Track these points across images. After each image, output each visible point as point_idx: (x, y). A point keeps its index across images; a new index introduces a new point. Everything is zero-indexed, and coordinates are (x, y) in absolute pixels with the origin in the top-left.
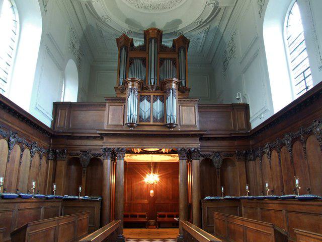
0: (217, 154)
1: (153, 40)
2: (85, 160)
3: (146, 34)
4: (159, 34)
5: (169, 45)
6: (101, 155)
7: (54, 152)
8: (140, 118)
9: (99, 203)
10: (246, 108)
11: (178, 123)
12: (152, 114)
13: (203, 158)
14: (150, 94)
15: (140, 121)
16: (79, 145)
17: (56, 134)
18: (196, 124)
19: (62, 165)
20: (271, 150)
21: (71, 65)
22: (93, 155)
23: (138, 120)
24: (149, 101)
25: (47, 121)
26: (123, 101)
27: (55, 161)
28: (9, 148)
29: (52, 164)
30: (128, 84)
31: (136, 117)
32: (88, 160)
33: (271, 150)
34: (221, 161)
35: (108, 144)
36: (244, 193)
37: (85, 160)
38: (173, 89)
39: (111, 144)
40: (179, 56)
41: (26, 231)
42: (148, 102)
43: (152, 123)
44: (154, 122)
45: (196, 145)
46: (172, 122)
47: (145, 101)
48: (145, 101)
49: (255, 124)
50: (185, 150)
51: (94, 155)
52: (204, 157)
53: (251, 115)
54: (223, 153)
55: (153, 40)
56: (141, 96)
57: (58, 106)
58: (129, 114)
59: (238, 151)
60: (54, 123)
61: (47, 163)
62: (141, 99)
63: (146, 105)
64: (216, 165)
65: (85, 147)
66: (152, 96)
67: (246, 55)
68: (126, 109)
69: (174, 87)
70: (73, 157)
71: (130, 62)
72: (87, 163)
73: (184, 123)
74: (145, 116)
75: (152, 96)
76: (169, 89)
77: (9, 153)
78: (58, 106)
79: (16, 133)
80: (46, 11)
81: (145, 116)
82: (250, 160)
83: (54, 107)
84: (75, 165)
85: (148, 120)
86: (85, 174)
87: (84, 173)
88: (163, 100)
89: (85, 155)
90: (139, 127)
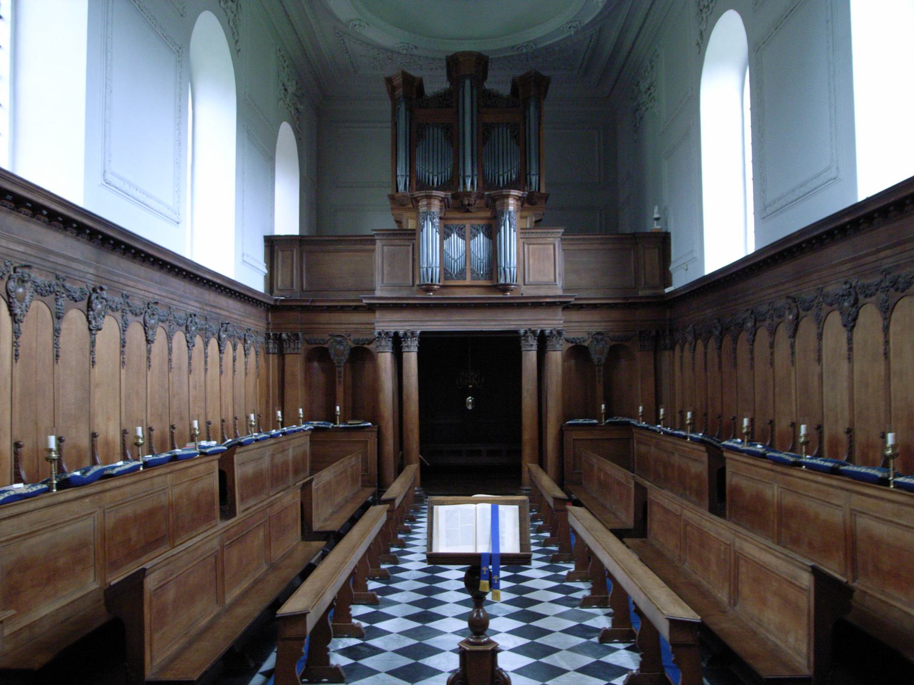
0: (598, 336)
1: (468, 83)
2: (340, 352)
3: (454, 63)
4: (481, 62)
5: (505, 90)
6: (370, 342)
7: (278, 339)
8: (446, 272)
9: (375, 434)
10: (663, 241)
11: (520, 282)
12: (468, 264)
13: (570, 345)
14: (464, 222)
15: (446, 279)
16: (327, 324)
17: (278, 304)
18: (555, 280)
19: (296, 364)
20: (696, 338)
21: (286, 134)
22: (354, 342)
23: (442, 276)
24: (462, 236)
25: (255, 280)
26: (412, 236)
27: (281, 354)
28: (220, 351)
29: (276, 361)
30: (418, 202)
31: (438, 270)
32: (347, 352)
33: (696, 338)
34: (606, 351)
35: (386, 324)
36: (635, 417)
37: (340, 352)
38: (510, 213)
39: (391, 324)
40: (525, 118)
41: (311, 486)
42: (460, 240)
43: (468, 282)
44: (473, 278)
45: (555, 322)
46: (508, 281)
47: (454, 236)
48: (454, 236)
49: (681, 279)
50: (534, 332)
51: (357, 341)
52: (572, 342)
53: (673, 257)
54: (611, 334)
55: (468, 83)
56: (446, 226)
57: (273, 244)
58: (425, 266)
59: (641, 332)
60: (270, 280)
61: (267, 362)
62: (445, 234)
63: (456, 244)
64: (595, 358)
65: (338, 326)
66: (468, 227)
67: (587, 289)
68: (416, 251)
69: (511, 208)
70: (315, 346)
71: (416, 137)
72: (344, 358)
73: (531, 280)
74: (456, 267)
75: (468, 227)
76: (503, 214)
77: (221, 359)
78: (273, 244)
79: (228, 323)
80: (239, 51)
81: (456, 267)
82: (665, 349)
83: (266, 246)
84: (319, 361)
85: (462, 274)
86: (342, 379)
87: (340, 377)
88: (492, 232)
89: (340, 343)
90: (445, 291)
